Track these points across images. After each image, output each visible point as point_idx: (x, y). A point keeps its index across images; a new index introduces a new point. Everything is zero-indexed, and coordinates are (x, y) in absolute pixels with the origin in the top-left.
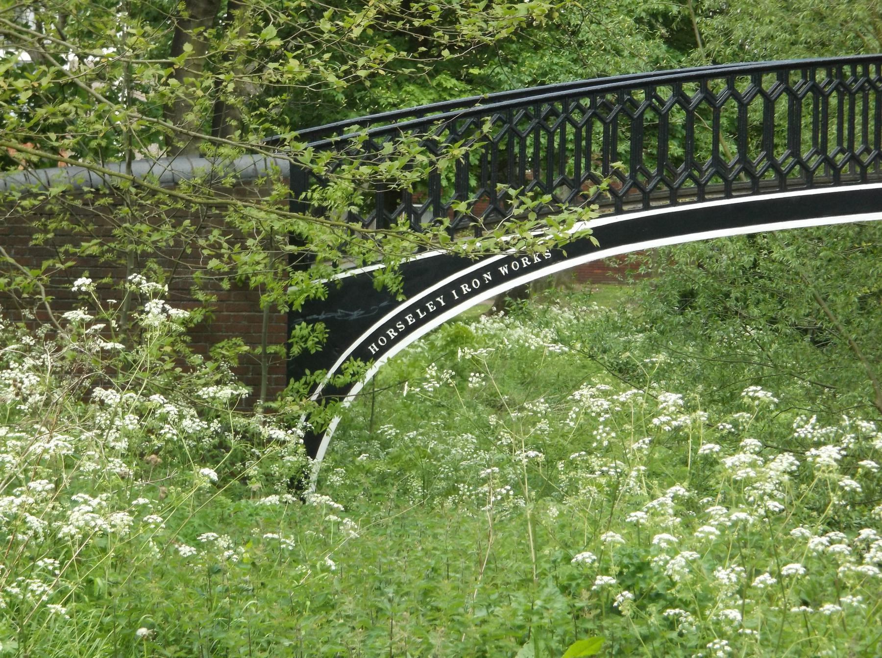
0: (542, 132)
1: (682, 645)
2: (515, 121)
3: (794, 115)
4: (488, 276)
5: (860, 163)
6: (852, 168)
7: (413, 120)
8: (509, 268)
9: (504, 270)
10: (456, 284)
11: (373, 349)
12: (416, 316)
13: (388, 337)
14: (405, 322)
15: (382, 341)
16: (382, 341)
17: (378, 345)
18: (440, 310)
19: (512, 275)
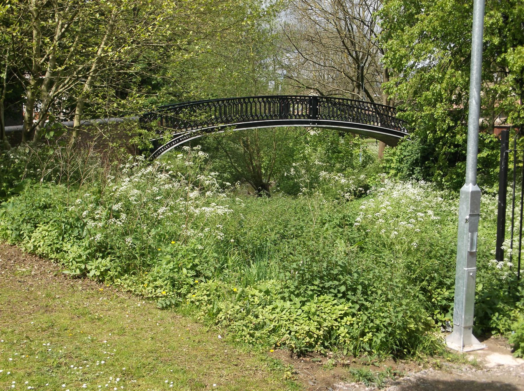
19: (183, 140)
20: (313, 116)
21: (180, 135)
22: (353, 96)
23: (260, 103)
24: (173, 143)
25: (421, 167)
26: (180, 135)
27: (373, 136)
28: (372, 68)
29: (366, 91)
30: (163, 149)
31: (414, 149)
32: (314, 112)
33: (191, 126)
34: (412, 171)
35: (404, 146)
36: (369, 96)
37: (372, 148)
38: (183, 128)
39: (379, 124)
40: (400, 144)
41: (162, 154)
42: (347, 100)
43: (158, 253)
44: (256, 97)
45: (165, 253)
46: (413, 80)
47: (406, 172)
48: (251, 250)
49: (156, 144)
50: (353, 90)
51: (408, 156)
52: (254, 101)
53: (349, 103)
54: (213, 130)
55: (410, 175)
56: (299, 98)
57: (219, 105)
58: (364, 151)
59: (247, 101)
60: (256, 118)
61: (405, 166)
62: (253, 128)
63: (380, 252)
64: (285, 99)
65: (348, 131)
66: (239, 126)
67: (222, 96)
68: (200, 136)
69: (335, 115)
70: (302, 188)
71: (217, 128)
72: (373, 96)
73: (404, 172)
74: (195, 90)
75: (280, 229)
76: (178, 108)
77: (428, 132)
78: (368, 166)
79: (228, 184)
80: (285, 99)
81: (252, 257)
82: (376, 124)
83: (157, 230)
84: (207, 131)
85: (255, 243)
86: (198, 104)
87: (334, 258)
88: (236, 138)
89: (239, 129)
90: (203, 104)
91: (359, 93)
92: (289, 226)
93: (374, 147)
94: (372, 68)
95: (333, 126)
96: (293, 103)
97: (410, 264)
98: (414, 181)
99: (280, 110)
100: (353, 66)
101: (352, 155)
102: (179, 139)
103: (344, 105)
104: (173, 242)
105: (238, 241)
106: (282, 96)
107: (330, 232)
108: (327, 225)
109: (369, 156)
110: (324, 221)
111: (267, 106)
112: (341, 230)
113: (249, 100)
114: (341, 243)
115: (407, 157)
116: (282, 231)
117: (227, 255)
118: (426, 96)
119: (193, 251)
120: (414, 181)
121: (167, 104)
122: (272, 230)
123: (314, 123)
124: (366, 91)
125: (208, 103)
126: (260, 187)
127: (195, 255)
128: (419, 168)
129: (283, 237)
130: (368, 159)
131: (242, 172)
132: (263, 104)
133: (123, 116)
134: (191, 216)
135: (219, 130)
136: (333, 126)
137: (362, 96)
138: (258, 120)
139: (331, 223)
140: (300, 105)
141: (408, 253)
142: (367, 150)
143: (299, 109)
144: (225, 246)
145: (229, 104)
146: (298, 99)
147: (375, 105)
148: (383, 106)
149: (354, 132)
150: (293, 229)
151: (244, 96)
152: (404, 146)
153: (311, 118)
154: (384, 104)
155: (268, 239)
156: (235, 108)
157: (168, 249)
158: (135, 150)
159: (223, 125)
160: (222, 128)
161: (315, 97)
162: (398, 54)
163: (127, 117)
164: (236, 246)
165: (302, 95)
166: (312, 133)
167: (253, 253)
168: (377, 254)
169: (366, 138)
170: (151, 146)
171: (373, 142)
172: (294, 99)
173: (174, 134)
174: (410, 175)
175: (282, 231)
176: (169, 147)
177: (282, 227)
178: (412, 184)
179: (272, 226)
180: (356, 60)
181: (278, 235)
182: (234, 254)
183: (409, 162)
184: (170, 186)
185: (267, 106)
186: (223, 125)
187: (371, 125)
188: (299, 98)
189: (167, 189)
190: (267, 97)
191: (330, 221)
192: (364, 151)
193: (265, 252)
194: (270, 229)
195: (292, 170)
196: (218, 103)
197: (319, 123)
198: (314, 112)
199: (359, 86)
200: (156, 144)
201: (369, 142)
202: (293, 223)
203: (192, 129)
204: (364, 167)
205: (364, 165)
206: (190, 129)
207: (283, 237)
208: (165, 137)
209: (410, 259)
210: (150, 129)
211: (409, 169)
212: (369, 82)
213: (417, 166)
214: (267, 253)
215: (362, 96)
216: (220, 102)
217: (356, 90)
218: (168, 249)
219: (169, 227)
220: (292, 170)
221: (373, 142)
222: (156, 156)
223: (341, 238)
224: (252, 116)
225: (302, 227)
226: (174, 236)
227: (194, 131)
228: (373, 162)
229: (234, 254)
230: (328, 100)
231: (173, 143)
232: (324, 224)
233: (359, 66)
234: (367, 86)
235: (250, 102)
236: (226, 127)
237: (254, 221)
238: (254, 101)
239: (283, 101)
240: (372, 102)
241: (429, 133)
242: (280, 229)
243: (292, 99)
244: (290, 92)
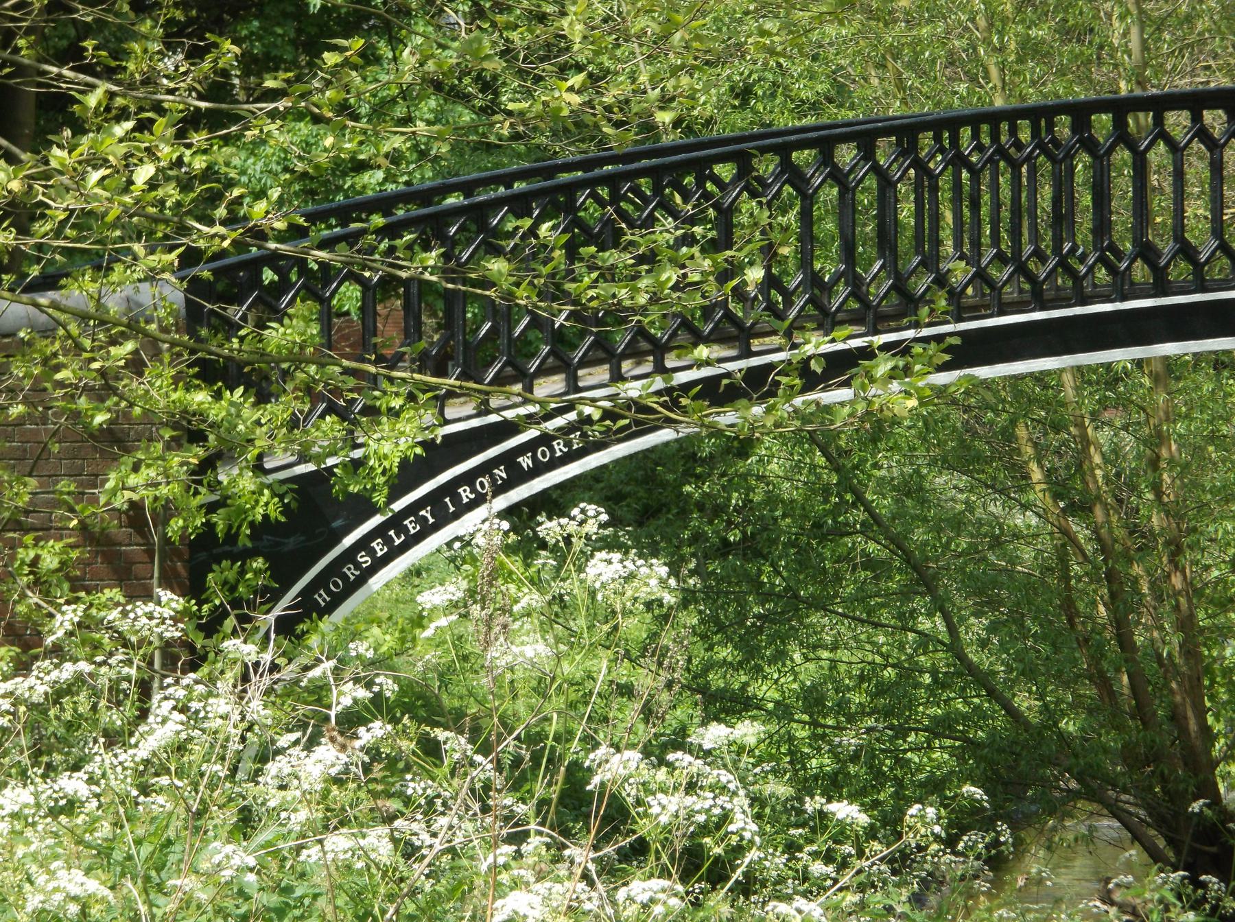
0: (1002, 164)
1: (775, 884)
2: (984, 262)
3: (928, 215)
4: (501, 473)
5: (990, 283)
6: (979, 293)
7: (416, 211)
8: (534, 458)
9: (526, 461)
10: (450, 488)
11: (322, 598)
12: (388, 541)
13: (345, 577)
14: (372, 552)
15: (336, 585)
16: (336, 585)
17: (329, 592)
18: (427, 531)
19: (539, 469)
21: (509, 429)
24: (465, 494)
26: (509, 429)
30: (379, 548)
33: (604, 353)
38: (543, 372)
41: (377, 582)
52: (1122, 136)
57: (876, 169)
60: (1140, 271)
62: (1120, 356)
67: (880, 96)
86: (675, 168)
88: (976, 445)
90: (743, 162)
102: (508, 459)
121: (426, 176)
125: (784, 151)
131: (1034, 718)
133: (49, 282)
135: (811, 381)
138: (1161, 286)
151: (1060, 89)
158: (120, 555)
159: (848, 340)
160: (840, 366)
163: (79, 291)
184: (378, 842)
186: (848, 340)
200: (316, 509)
203: (617, 377)
206: (601, 373)
222: (322, 598)
224: (1108, 255)
236: (867, 353)
238: (1122, 136)
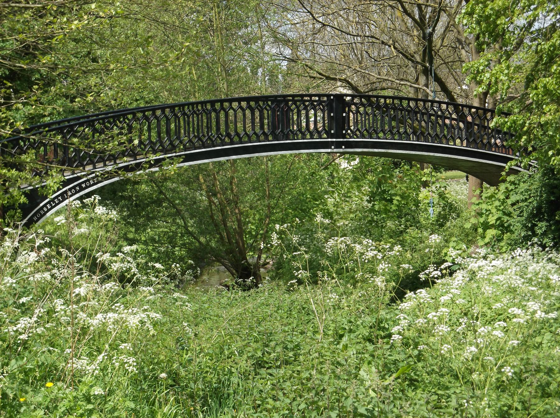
19: (87, 187)
20: (336, 131)
22: (417, 90)
23: (243, 110)
25: (548, 221)
27: (451, 166)
28: (451, 36)
29: (438, 80)
31: (533, 187)
32: (338, 125)
34: (532, 229)
35: (513, 183)
36: (444, 89)
37: (458, 188)
39: (465, 142)
40: (504, 181)
42: (409, 99)
43: (21, 406)
44: (226, 101)
45: (32, 407)
46: (523, 58)
47: (519, 232)
48: (201, 393)
49: (34, 196)
50: (417, 80)
51: (523, 201)
53: (412, 104)
54: (138, 166)
55: (527, 238)
56: (317, 98)
58: (442, 196)
59: (218, 106)
61: (517, 224)
63: (447, 388)
64: (280, 102)
65: (409, 160)
66: (189, 158)
67: (167, 98)
68: (116, 179)
69: (387, 127)
70: (298, 269)
71: (146, 162)
72: (456, 90)
73: (516, 233)
74: (108, 91)
75: (255, 350)
76: (67, 127)
77: (550, 153)
78: (448, 224)
79: (158, 265)
80: (280, 102)
81: (203, 406)
82: (458, 141)
83: (20, 363)
84: (127, 169)
85: (208, 379)
86: (116, 115)
87: (350, 401)
88: (189, 180)
89: (187, 164)
90: (134, 114)
91: (427, 85)
92: (272, 344)
93: (460, 187)
94: (451, 36)
95: (376, 150)
96: (297, 107)
97: (505, 408)
98: (536, 249)
99: (273, 123)
100: (416, 33)
101: (417, 203)
103: (395, 109)
104: (49, 384)
105: (175, 377)
106: (276, 97)
107: (351, 352)
108: (345, 340)
109: (451, 205)
110: (341, 332)
111: (257, 114)
112: (370, 347)
113: (222, 105)
114: (369, 372)
115: (521, 204)
116: (259, 354)
117: (153, 404)
118: (545, 87)
119: (88, 399)
120: (536, 249)
122: (241, 353)
123: (338, 145)
124: (438, 80)
126: (245, 274)
127: (90, 407)
128: (544, 224)
129: (260, 364)
130: (450, 210)
132: (248, 112)
134: (84, 330)
135: (151, 166)
136: (376, 150)
137: (432, 91)
138: (232, 143)
139: (352, 336)
140: (320, 114)
141: (501, 387)
142: (446, 192)
143: (316, 119)
144: (150, 386)
145: (176, 115)
146: (315, 101)
147: (457, 107)
148: (471, 107)
149: (422, 161)
150: (279, 349)
152: (513, 183)
153: (332, 136)
154: (476, 103)
155: (233, 370)
156: (197, 124)
157: (39, 398)
160: (158, 162)
161: (340, 97)
162: (490, 7)
164: (171, 386)
165: (322, 92)
166: (344, 164)
167: (205, 398)
168: (440, 392)
169: (446, 170)
170: (23, 199)
171: (461, 177)
172: (300, 100)
173: (68, 175)
174: (527, 238)
175: (259, 354)
176: (60, 202)
177: (259, 345)
178: (533, 255)
179: (240, 344)
180: (421, 24)
181: (251, 362)
182: (167, 401)
183: (525, 214)
184: (47, 275)
185: (257, 114)
187: (451, 145)
188: (317, 98)
189: (39, 282)
190: (256, 99)
191: (351, 331)
192: (442, 196)
193: (229, 395)
194: (239, 353)
195: (275, 236)
196: (154, 114)
197: (349, 145)
198: (338, 125)
199: (426, 72)
200: (34, 196)
201: (452, 178)
202: (280, 337)
203: (105, 165)
204: (442, 225)
205: (440, 223)
206: (101, 164)
207: (260, 364)
208: (49, 182)
209: (505, 399)
210: (20, 167)
211: (525, 226)
212: (445, 63)
213: (540, 220)
214: (231, 397)
215: (432, 91)
216: (167, 110)
217: (422, 80)
218: (39, 398)
219: (43, 355)
220: (275, 236)
221: (461, 177)
223: (369, 363)
225: (298, 346)
226: (50, 373)
227: (109, 168)
228: (458, 216)
229: (167, 401)
230: (368, 99)
231: (69, 193)
232: (341, 336)
233: (424, 34)
234: (443, 73)
235: (224, 110)
236: (164, 159)
237: (207, 338)
238: (222, 108)
239: (278, 105)
240: (452, 101)
241: (553, 155)
242: (255, 350)
243: (295, 102)
244: (297, 87)
